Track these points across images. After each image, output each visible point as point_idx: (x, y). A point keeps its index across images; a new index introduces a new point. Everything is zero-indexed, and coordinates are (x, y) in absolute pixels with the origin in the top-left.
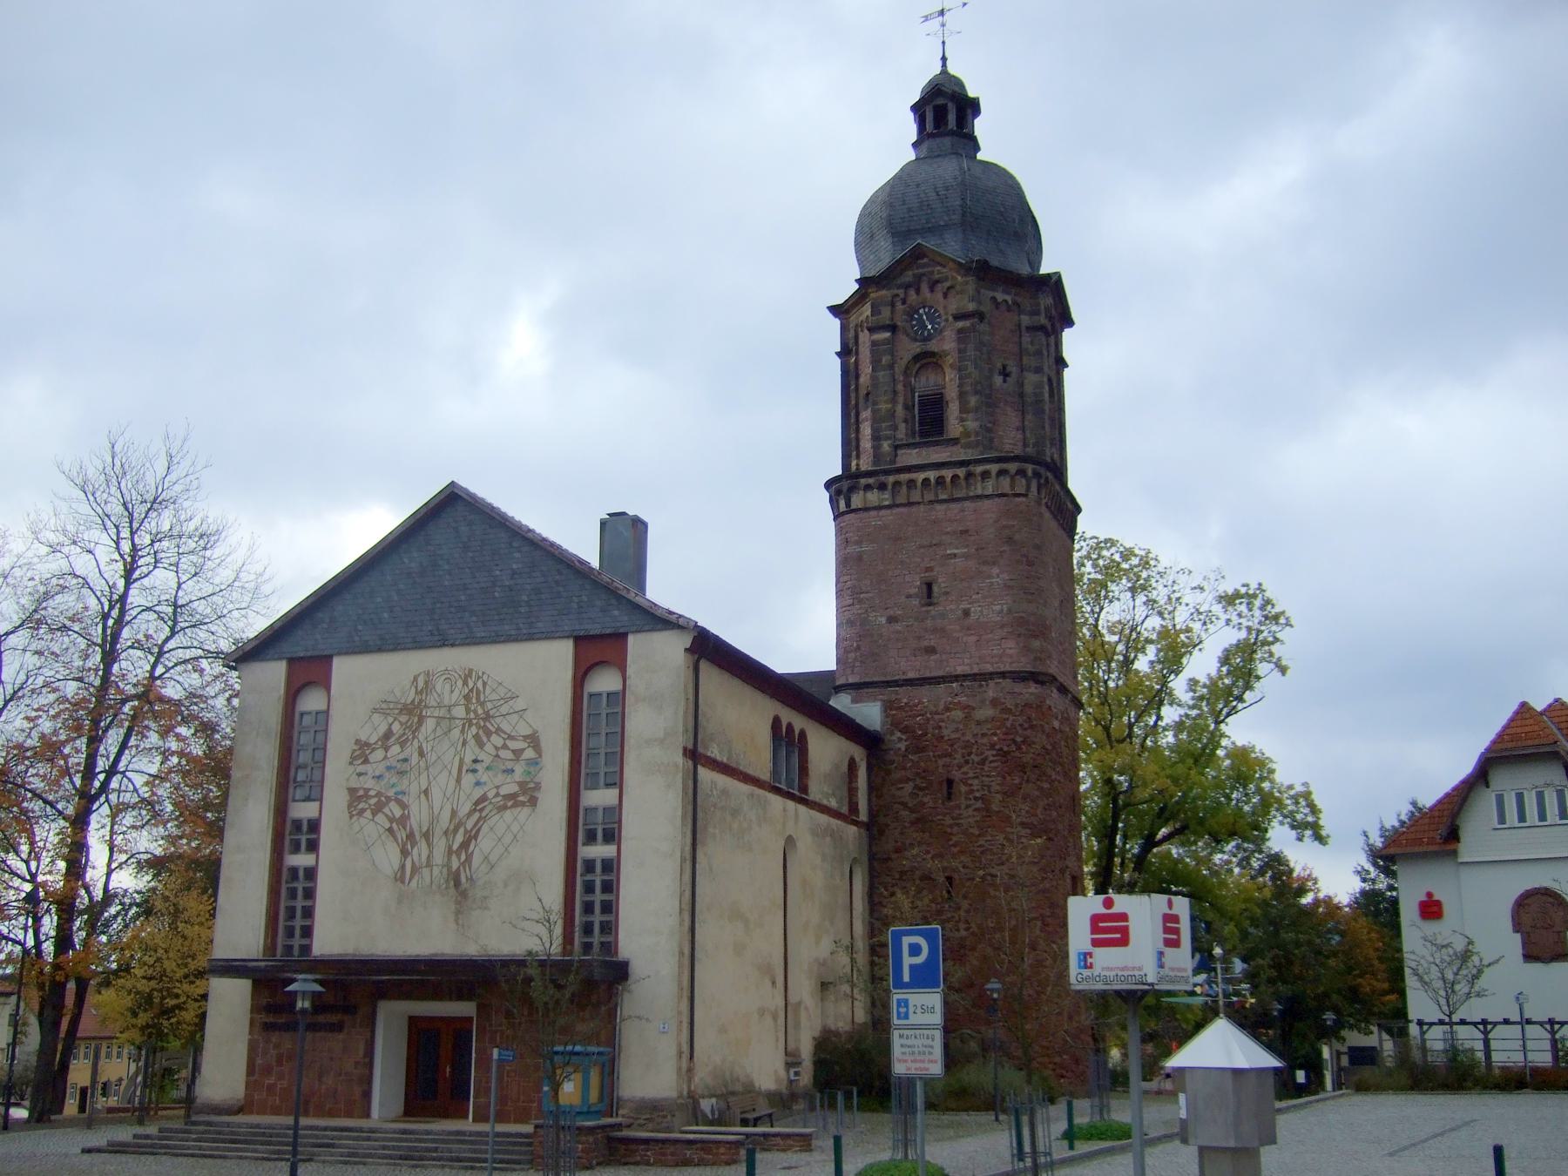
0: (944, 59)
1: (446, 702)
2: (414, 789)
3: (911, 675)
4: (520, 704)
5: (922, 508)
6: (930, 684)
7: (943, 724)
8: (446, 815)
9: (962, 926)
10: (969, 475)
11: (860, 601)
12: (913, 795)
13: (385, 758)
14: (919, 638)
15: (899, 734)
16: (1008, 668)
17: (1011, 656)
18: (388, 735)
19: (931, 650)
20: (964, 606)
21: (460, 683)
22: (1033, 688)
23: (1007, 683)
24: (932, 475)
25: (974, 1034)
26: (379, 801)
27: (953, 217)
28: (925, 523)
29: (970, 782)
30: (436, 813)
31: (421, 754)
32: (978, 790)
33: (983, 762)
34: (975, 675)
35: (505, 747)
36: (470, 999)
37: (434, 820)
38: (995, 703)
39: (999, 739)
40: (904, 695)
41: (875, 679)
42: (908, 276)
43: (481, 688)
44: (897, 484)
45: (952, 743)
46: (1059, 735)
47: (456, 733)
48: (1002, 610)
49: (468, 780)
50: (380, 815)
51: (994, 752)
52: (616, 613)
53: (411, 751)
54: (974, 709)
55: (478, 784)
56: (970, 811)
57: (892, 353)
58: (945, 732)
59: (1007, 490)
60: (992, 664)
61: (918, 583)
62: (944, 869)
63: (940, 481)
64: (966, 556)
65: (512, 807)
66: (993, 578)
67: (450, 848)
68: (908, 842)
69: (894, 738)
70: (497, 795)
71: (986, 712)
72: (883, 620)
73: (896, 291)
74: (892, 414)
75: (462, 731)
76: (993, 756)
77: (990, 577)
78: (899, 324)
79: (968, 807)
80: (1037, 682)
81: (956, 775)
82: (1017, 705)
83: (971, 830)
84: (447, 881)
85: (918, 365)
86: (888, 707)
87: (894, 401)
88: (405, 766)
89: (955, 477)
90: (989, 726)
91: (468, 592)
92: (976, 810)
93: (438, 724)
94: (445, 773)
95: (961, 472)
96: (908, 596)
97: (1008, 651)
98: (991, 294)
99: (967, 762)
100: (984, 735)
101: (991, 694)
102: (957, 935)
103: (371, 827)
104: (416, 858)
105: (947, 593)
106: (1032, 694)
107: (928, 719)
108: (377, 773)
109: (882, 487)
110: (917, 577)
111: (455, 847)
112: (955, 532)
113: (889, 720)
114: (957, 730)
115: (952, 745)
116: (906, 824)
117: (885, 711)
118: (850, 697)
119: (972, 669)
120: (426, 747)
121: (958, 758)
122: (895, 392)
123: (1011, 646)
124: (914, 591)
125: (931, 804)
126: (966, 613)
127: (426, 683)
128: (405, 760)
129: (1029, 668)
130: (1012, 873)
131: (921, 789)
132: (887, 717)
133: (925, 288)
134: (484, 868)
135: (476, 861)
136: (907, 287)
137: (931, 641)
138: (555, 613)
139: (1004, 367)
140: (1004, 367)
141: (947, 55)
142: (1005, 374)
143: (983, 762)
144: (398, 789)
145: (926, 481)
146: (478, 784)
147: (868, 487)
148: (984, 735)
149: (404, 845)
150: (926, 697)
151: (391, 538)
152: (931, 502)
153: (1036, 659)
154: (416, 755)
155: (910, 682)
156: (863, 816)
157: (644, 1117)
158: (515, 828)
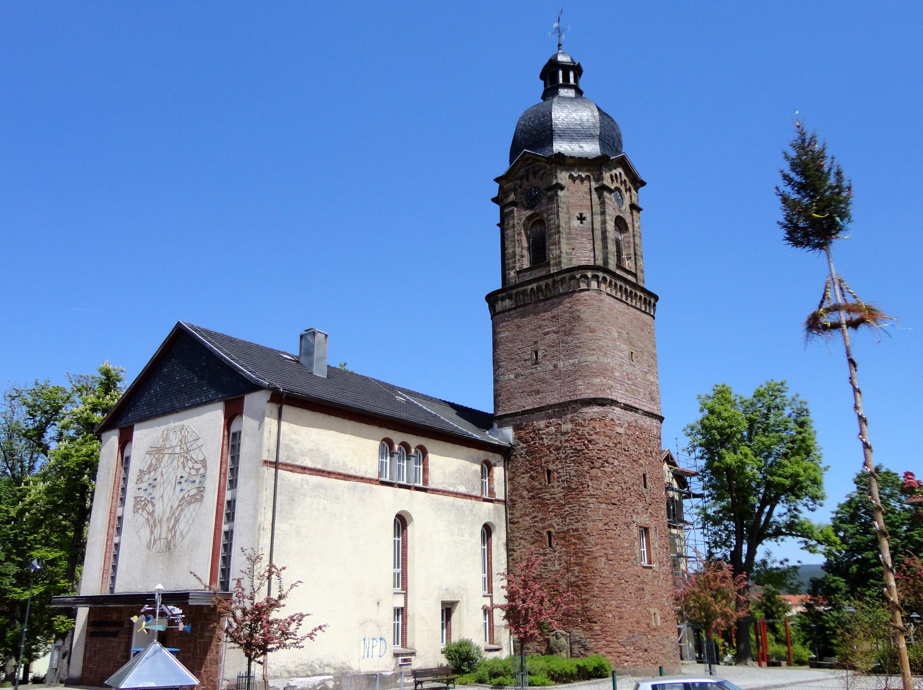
4: (200, 442)
7: (544, 436)
8: (168, 510)
9: (556, 562)
10: (554, 282)
18: (151, 464)
24: (534, 286)
25: (564, 633)
35: (193, 468)
45: (549, 447)
46: (625, 437)
49: (178, 487)
51: (572, 451)
62: (544, 528)
63: (539, 288)
65: (194, 502)
70: (188, 496)
72: (512, 376)
73: (516, 182)
75: (178, 461)
76: (572, 453)
79: (559, 486)
81: (551, 467)
83: (561, 501)
85: (531, 222)
89: (547, 285)
92: (563, 488)
94: (170, 485)
95: (550, 281)
100: (567, 441)
103: (142, 517)
105: (545, 356)
106: (594, 413)
112: (548, 319)
113: (517, 436)
126: (555, 366)
128: (156, 479)
133: (531, 177)
136: (521, 178)
137: (537, 387)
139: (581, 214)
140: (581, 214)
142: (581, 218)
143: (566, 458)
144: (152, 496)
146: (181, 490)
147: (503, 299)
156: (500, 494)
158: (194, 514)
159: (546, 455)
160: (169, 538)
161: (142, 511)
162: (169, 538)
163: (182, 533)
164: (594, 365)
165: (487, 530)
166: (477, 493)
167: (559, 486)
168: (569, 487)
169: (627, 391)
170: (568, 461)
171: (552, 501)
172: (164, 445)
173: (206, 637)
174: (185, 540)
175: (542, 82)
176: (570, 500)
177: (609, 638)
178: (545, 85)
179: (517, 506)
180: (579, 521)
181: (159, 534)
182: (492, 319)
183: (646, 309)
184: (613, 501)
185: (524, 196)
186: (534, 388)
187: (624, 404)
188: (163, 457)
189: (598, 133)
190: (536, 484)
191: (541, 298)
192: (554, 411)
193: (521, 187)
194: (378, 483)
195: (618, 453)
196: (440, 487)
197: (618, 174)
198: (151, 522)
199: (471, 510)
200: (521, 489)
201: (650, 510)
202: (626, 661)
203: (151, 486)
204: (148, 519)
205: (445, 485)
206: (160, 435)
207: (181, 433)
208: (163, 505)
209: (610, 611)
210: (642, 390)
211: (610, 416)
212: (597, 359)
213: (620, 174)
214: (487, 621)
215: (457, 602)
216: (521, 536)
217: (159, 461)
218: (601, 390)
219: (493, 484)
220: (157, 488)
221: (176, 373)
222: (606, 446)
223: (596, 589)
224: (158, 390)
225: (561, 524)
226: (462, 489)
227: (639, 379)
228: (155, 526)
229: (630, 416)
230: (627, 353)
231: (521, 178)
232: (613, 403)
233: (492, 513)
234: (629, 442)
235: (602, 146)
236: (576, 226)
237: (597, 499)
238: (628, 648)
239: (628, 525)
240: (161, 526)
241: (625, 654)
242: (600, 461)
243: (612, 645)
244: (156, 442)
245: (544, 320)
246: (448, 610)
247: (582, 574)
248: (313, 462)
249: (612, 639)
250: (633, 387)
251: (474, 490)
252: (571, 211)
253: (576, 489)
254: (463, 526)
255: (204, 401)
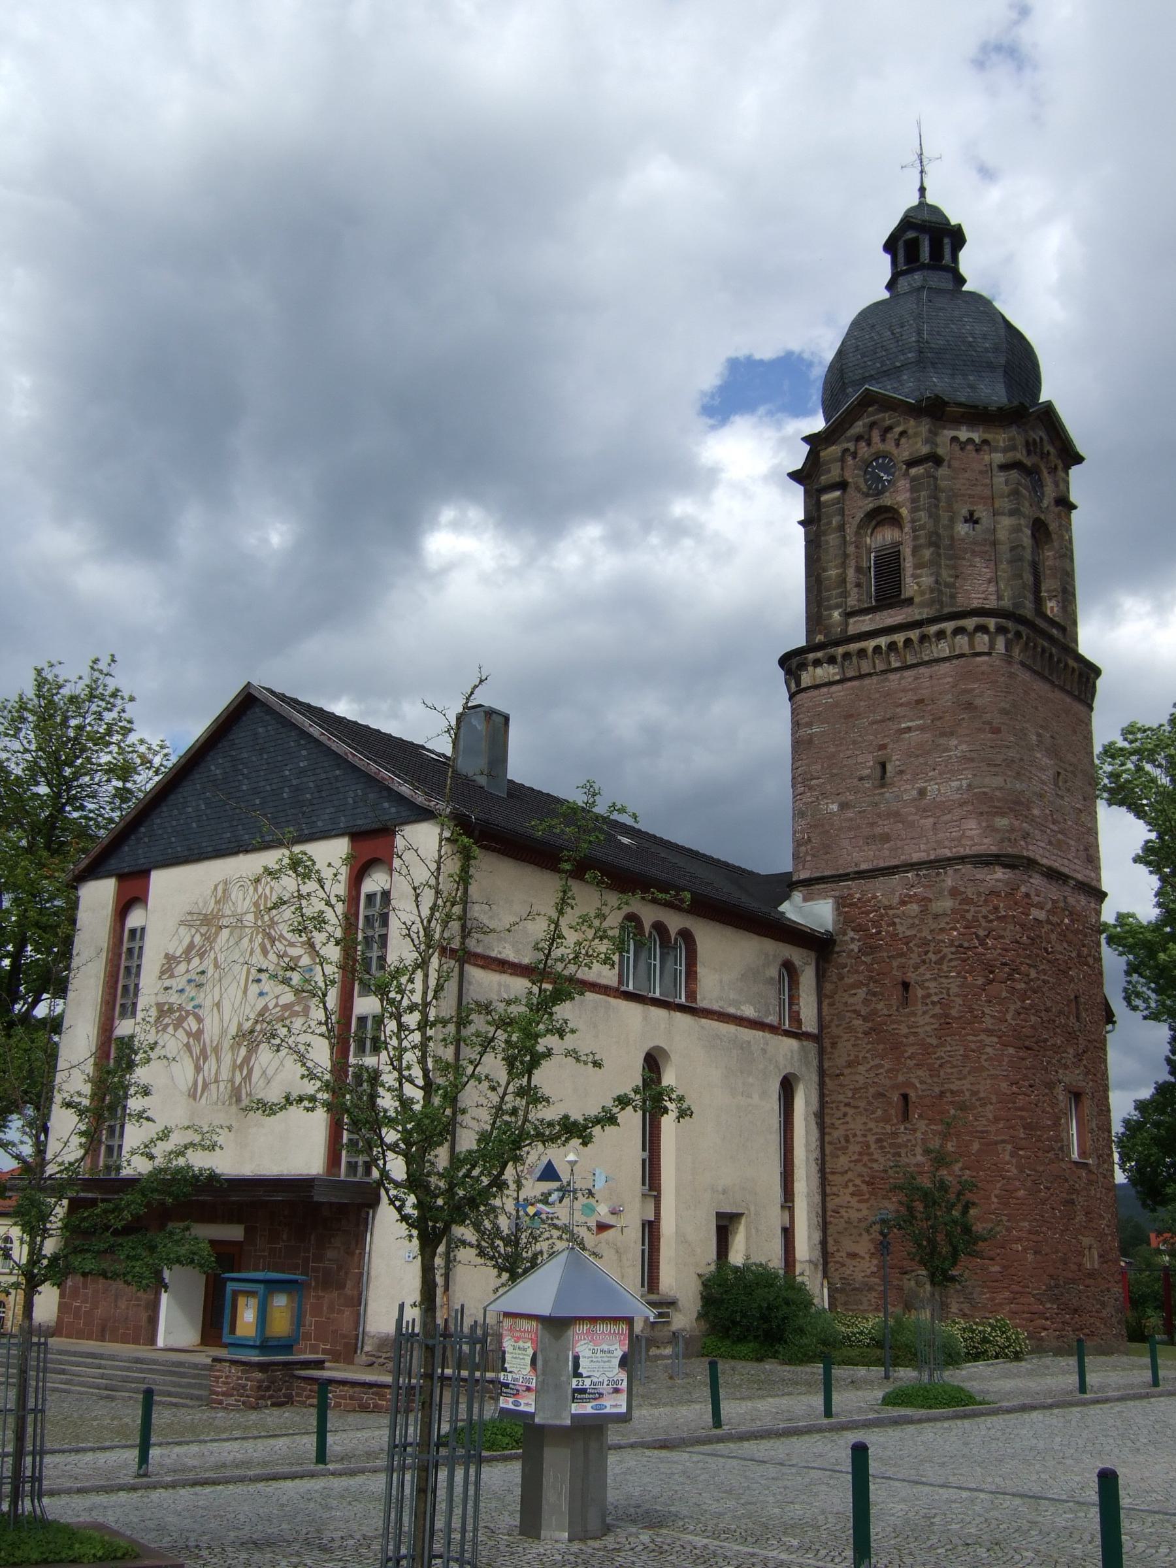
0: (922, 190)
1: (239, 911)
2: (208, 1003)
3: (864, 867)
5: (875, 679)
6: (883, 875)
7: (897, 920)
10: (924, 638)
11: (811, 788)
12: (866, 1002)
13: (188, 971)
14: (872, 824)
15: (851, 934)
16: (968, 852)
17: (972, 838)
18: (191, 946)
19: (886, 838)
20: (920, 784)
21: (251, 889)
22: (1000, 874)
23: (967, 869)
24: (883, 641)
26: (181, 1015)
27: (910, 355)
28: (877, 695)
29: (926, 984)
30: (225, 1025)
31: (216, 966)
32: (936, 994)
33: (940, 962)
34: (931, 862)
36: (239, 1222)
37: (223, 1032)
38: (954, 892)
39: (959, 934)
40: (856, 890)
41: (826, 874)
42: (859, 427)
43: (268, 893)
44: (846, 656)
45: (907, 940)
46: (1047, 927)
47: (246, 941)
48: (961, 786)
49: (254, 989)
50: (180, 1030)
51: (953, 949)
52: (386, 805)
53: (208, 964)
54: (930, 900)
55: (261, 994)
56: (927, 1018)
57: (842, 512)
58: (900, 929)
59: (966, 650)
60: (950, 848)
61: (871, 763)
62: (895, 1087)
63: (892, 646)
64: (921, 729)
66: (951, 750)
67: (235, 1061)
68: (861, 1055)
69: (846, 938)
70: (276, 1005)
71: (946, 904)
72: (834, 807)
73: (846, 445)
74: (843, 581)
75: (251, 941)
77: (947, 750)
78: (850, 480)
79: (924, 1013)
80: (1005, 866)
81: (911, 977)
82: (979, 894)
83: (928, 1040)
84: (231, 1097)
85: (874, 523)
86: (841, 904)
87: (843, 565)
88: (202, 979)
89: (908, 641)
90: (948, 919)
91: (262, 795)
92: (933, 1016)
93: (231, 933)
94: (235, 984)
96: (861, 779)
97: (968, 833)
98: (953, 433)
99: (924, 962)
100: (942, 930)
101: (949, 882)
102: (913, 1161)
104: (206, 1074)
105: (902, 772)
106: (997, 880)
107: (882, 916)
108: (180, 988)
109: (832, 660)
110: (871, 757)
111: (239, 1062)
112: (908, 704)
113: (841, 918)
114: (913, 926)
115: (907, 944)
116: (860, 1035)
117: (838, 909)
118: (800, 895)
119: (929, 855)
120: (221, 959)
121: (915, 958)
122: (846, 556)
123: (972, 826)
124: (866, 772)
125: (885, 1012)
126: (922, 793)
127: (224, 891)
128: (203, 973)
129: (994, 850)
130: (974, 1088)
131: (874, 994)
132: (839, 915)
133: (876, 436)
134: (262, 1083)
135: (256, 1074)
137: (883, 827)
138: (333, 810)
139: (971, 513)
140: (971, 513)
141: (926, 185)
143: (940, 962)
144: (196, 1002)
145: (877, 649)
146: (261, 994)
147: (817, 663)
148: (942, 930)
149: (198, 1059)
150: (883, 891)
151: (198, 745)
152: (883, 672)
153: (1002, 841)
154: (212, 966)
155: (861, 875)
156: (810, 1024)
157: (384, 1355)
159: (902, 955)
160: (238, 1079)
161: (175, 1030)
162: (238, 1079)
163: (264, 1072)
164: (998, 793)
165: (787, 1087)
166: (772, 1019)
167: (924, 1013)
168: (947, 1016)
169: (1050, 843)
170: (945, 968)
171: (912, 1039)
172: (219, 910)
173: (329, 1260)
174: (273, 1084)
175: (887, 258)
176: (948, 1039)
177: (1015, 1287)
178: (894, 263)
179: (840, 1045)
180: (965, 1078)
181: (213, 1072)
182: (790, 699)
183: (1080, 692)
184: (1027, 1043)
185: (861, 473)
186: (878, 830)
187: (1050, 868)
188: (217, 934)
189: (1002, 360)
190: (880, 1006)
191: (895, 664)
192: (918, 875)
193: (854, 455)
194: (617, 994)
195: (1037, 955)
196: (715, 1007)
197: (1038, 440)
198: (196, 1050)
199: (764, 1051)
200: (848, 1014)
201: (1085, 1062)
202: (1045, 1329)
203: (193, 984)
204: (187, 1045)
205: (721, 1003)
206: (209, 892)
207: (256, 890)
208: (222, 1020)
209: (1019, 1240)
210: (1072, 843)
211: (1023, 889)
212: (1003, 784)
213: (1041, 439)
214: (646, 1247)
215: (740, 1215)
216: (847, 1100)
217: (209, 939)
218: (1010, 840)
219: (798, 1004)
220: (208, 988)
221: (240, 777)
222: (1018, 942)
223: (995, 1200)
224: (203, 807)
225: (929, 1081)
226: (749, 1011)
227: (1070, 823)
228: (206, 1059)
229: (1053, 892)
230: (1050, 773)
231: (859, 438)
232: (1030, 864)
233: (796, 1057)
234: (1053, 936)
235: (1009, 387)
236: (963, 533)
237: (1000, 1037)
238: (1048, 1305)
239: (1051, 1086)
240: (218, 1060)
241: (1042, 1315)
242: (1007, 969)
243: (1022, 1300)
244: (201, 905)
245: (901, 705)
246: (725, 1225)
247: (968, 1172)
248: (517, 951)
249: (1020, 1289)
250: (1060, 836)
251: (768, 1013)
252: (955, 506)
253: (960, 1018)
254: (751, 1080)
255: (306, 832)
